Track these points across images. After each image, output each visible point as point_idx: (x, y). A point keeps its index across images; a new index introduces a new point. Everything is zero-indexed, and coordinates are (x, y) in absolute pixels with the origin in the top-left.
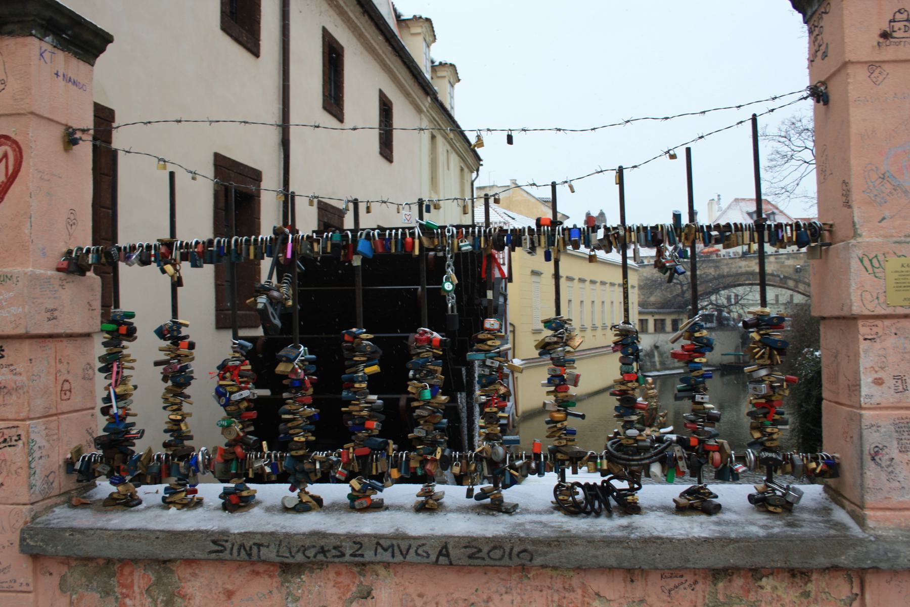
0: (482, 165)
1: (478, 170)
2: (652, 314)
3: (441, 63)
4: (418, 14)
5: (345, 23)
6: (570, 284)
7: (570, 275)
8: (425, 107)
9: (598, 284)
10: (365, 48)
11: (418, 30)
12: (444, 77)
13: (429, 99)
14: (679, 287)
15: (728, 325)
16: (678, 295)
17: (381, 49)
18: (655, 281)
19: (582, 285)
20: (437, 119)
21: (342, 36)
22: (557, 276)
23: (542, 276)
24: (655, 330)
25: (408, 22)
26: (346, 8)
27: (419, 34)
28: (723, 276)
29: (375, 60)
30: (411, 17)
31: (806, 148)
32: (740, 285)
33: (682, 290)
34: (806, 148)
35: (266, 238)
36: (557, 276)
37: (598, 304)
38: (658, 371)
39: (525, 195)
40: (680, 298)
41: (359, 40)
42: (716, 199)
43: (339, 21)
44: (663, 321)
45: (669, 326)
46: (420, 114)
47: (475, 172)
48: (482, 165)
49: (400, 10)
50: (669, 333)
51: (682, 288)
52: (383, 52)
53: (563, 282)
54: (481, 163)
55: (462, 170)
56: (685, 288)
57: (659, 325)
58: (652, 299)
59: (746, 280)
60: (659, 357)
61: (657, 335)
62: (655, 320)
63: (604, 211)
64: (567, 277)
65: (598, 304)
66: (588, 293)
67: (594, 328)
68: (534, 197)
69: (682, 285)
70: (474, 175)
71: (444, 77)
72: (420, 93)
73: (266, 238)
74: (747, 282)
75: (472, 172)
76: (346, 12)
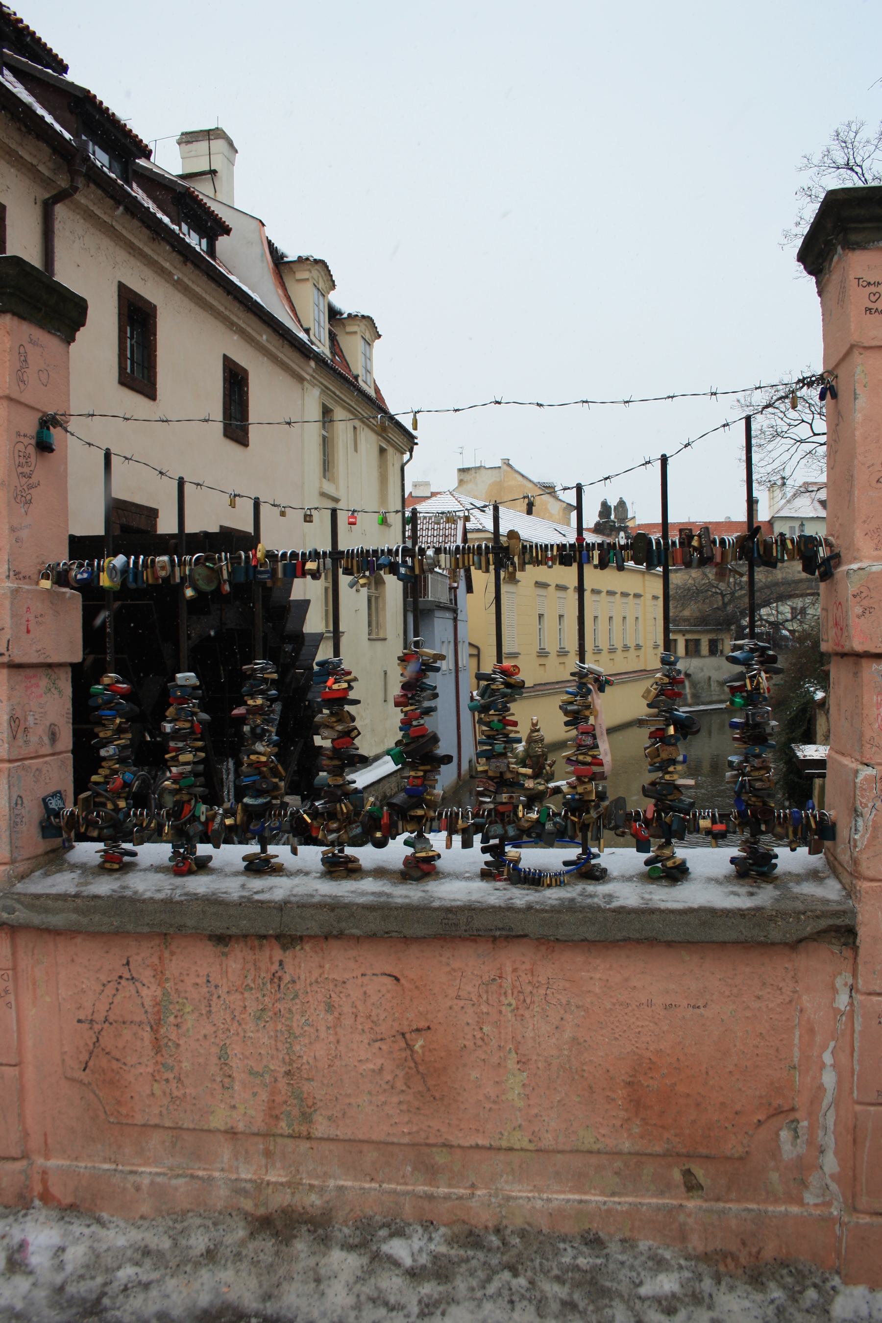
0: (417, 444)
1: (411, 451)
2: (683, 633)
3: (350, 315)
4: (304, 254)
5: (159, 275)
6: (596, 597)
7: (596, 587)
8: (308, 374)
9: (618, 596)
10: (197, 304)
11: (305, 275)
12: (355, 333)
13: (312, 364)
14: (720, 597)
15: (786, 646)
16: (718, 608)
17: (222, 305)
18: (689, 589)
19: (611, 599)
20: (331, 387)
21: (244, 357)
22: (581, 589)
23: (519, 584)
24: (687, 653)
25: (291, 265)
26: (156, 257)
27: (307, 280)
28: (776, 584)
29: (216, 318)
30: (296, 259)
31: (803, 421)
32: (797, 596)
33: (723, 603)
34: (803, 421)
35: (353, 550)
36: (581, 589)
37: (617, 620)
38: (690, 706)
39: (520, 478)
40: (720, 612)
41: (185, 295)
42: (779, 482)
43: (148, 273)
44: (697, 642)
45: (705, 648)
46: (302, 383)
47: (408, 453)
48: (417, 444)
49: (281, 246)
50: (704, 657)
51: (723, 599)
52: (226, 308)
53: (587, 595)
54: (416, 441)
55: (382, 451)
56: (726, 600)
57: (691, 646)
58: (686, 613)
59: (808, 589)
60: (690, 688)
61: (688, 660)
62: (687, 641)
63: (625, 499)
64: (557, 586)
65: (617, 620)
66: (618, 608)
67: (612, 650)
68: (530, 481)
69: (723, 596)
70: (407, 456)
71: (355, 333)
72: (296, 356)
73: (353, 550)
74: (808, 591)
75: (403, 453)
76: (157, 262)
